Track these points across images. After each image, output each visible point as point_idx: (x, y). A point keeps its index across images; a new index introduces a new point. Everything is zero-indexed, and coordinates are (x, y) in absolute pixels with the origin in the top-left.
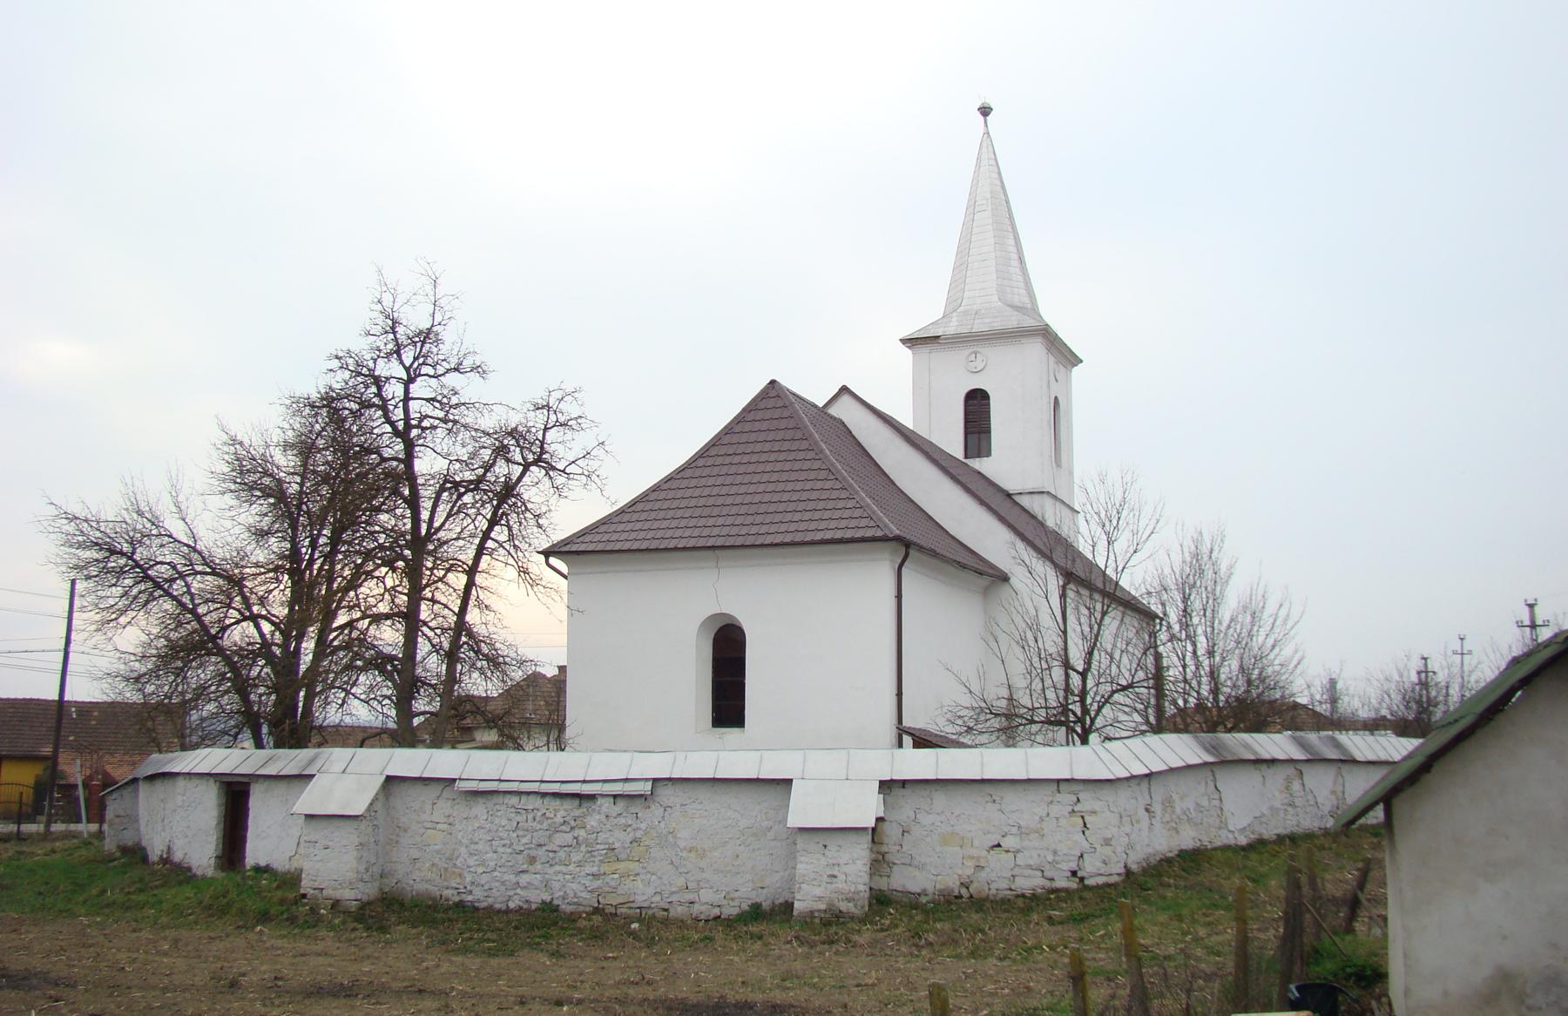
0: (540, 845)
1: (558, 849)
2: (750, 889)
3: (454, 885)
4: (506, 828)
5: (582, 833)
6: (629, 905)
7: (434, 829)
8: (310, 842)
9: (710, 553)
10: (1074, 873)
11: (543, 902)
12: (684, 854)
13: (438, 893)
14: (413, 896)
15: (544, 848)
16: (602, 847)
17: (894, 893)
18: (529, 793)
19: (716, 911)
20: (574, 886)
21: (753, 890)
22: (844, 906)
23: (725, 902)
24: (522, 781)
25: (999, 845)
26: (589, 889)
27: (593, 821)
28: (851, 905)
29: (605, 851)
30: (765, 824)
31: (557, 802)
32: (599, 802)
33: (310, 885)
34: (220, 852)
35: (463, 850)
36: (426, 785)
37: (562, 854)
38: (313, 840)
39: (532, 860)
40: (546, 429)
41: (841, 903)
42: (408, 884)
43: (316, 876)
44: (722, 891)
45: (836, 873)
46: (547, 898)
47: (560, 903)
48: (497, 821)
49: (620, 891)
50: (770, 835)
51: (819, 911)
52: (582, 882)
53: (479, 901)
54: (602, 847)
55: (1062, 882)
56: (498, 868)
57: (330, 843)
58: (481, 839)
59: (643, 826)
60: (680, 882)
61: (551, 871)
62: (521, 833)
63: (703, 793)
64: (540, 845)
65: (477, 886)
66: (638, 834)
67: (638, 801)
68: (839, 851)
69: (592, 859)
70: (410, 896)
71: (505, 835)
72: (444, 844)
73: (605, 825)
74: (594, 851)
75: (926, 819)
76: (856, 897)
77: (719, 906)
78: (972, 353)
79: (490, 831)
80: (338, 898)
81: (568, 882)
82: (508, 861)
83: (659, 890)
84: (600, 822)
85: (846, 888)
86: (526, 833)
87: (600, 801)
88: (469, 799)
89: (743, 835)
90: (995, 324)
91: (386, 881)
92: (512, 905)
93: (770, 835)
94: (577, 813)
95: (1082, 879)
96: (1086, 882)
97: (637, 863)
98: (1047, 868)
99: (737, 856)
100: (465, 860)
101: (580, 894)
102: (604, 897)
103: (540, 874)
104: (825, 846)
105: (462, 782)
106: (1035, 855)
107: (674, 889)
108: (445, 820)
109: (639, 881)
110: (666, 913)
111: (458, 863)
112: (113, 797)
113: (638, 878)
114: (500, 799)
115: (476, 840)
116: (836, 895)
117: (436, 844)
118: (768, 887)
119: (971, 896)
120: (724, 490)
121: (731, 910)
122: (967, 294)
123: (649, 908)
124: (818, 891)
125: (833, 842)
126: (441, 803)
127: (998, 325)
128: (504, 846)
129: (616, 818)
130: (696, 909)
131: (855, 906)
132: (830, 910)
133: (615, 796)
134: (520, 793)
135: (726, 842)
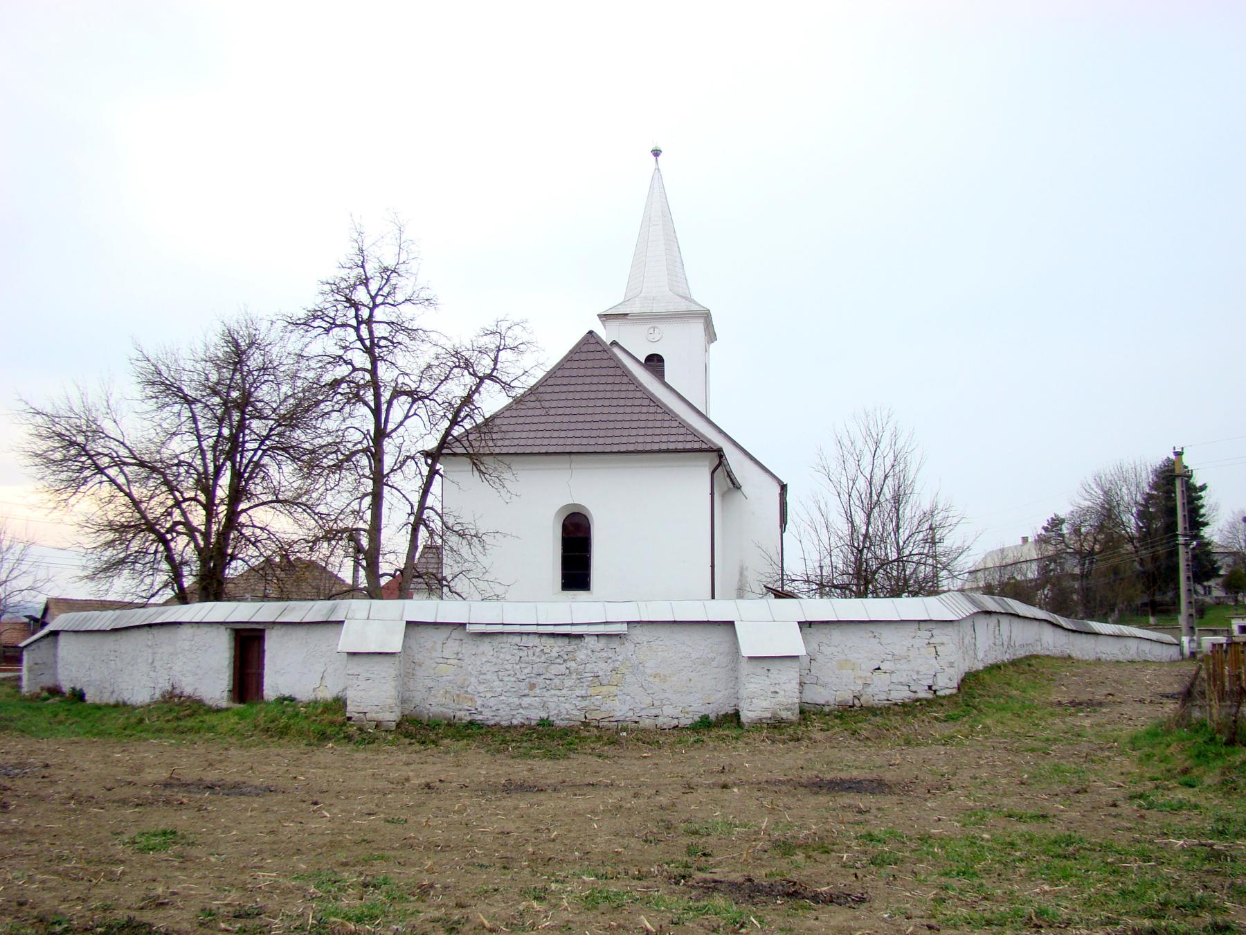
0: (539, 675)
1: (553, 677)
3: (467, 707)
5: (573, 664)
7: (446, 663)
9: (567, 457)
10: (930, 687)
11: (542, 719)
12: (651, 679)
13: (452, 714)
14: (429, 717)
16: (589, 675)
19: (675, 722)
20: (567, 706)
22: (785, 714)
24: (521, 625)
25: (879, 669)
27: (581, 655)
31: (551, 641)
33: (355, 710)
34: (231, 687)
35: (473, 679)
37: (557, 681)
39: (532, 686)
40: (499, 350)
41: (782, 712)
45: (778, 690)
46: (544, 715)
48: (502, 656)
49: (602, 709)
50: (715, 664)
51: (766, 718)
53: (488, 719)
54: (589, 675)
55: (923, 694)
57: (372, 676)
59: (620, 658)
60: (648, 701)
62: (523, 665)
63: (662, 632)
64: (539, 675)
71: (509, 667)
75: (826, 650)
76: (793, 707)
78: (651, 327)
79: (496, 664)
80: (380, 719)
81: (562, 702)
83: (632, 707)
87: (587, 639)
92: (515, 722)
93: (715, 664)
94: (570, 649)
95: (935, 691)
96: (938, 693)
98: (912, 683)
99: (690, 680)
101: (571, 712)
102: (590, 714)
104: (768, 670)
105: (471, 626)
106: (905, 675)
107: (643, 706)
108: (455, 656)
111: (468, 690)
112: (32, 648)
113: (616, 698)
114: (504, 638)
115: (485, 671)
118: (713, 703)
119: (862, 706)
121: (685, 722)
124: (765, 704)
126: (450, 643)
127: (672, 308)
128: (509, 675)
130: (661, 721)
132: (774, 717)
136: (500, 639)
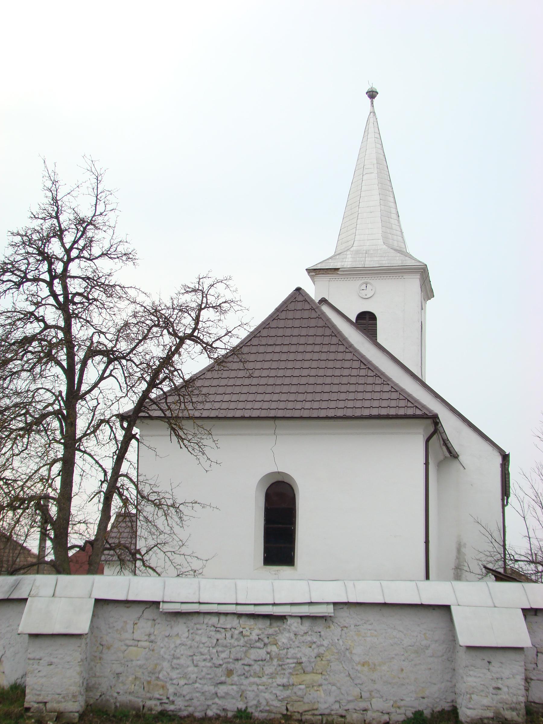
0: (237, 660)
1: (252, 663)
2: (413, 699)
4: (206, 645)
5: (274, 649)
6: (313, 712)
8: (34, 659)
11: (239, 711)
12: (359, 668)
13: (141, 704)
14: (116, 707)
15: (241, 662)
17: (533, 704)
18: (226, 614)
19: (386, 718)
20: (267, 696)
21: (416, 699)
23: (393, 710)
26: (280, 698)
27: (283, 639)
28: (514, 713)
29: (294, 665)
30: (424, 643)
31: (251, 622)
32: (289, 622)
35: (166, 664)
36: (128, 607)
38: (38, 657)
39: (230, 673)
42: (112, 696)
43: (41, 691)
44: (390, 700)
45: (500, 686)
47: (253, 711)
48: (198, 638)
49: (306, 700)
50: (429, 652)
51: (488, 718)
52: (274, 692)
53: (180, 710)
56: (198, 680)
57: (55, 660)
58: (182, 655)
59: (325, 643)
60: (356, 691)
61: (246, 682)
62: (220, 649)
63: (372, 616)
64: (237, 660)
65: (179, 697)
66: (322, 650)
67: (321, 622)
68: (501, 667)
69: (282, 672)
70: (113, 707)
71: (203, 650)
72: (147, 659)
73: (294, 642)
74: (284, 665)
76: (518, 707)
77: (388, 713)
79: (191, 647)
82: (208, 674)
83: (338, 699)
84: (290, 639)
85: (510, 699)
86: (225, 649)
87: (290, 621)
88: (169, 619)
89: (407, 652)
90: (384, 262)
91: (91, 694)
92: (210, 713)
93: (429, 652)
94: (271, 631)
97: (320, 676)
99: (402, 670)
100: (168, 674)
101: (271, 703)
102: (292, 705)
103: (237, 685)
104: (489, 662)
107: (350, 698)
109: (322, 691)
110: (343, 719)
111: (161, 676)
114: (201, 619)
115: (179, 655)
116: (501, 705)
117: (138, 660)
118: (428, 697)
120: (273, 373)
122: (357, 237)
123: (329, 715)
124: (486, 701)
125: (497, 658)
126: (142, 623)
127: (386, 263)
128: (204, 660)
129: (302, 636)
131: (518, 715)
132: (497, 717)
133: (301, 617)
134: (218, 614)
135: (393, 658)
136: (195, 619)
